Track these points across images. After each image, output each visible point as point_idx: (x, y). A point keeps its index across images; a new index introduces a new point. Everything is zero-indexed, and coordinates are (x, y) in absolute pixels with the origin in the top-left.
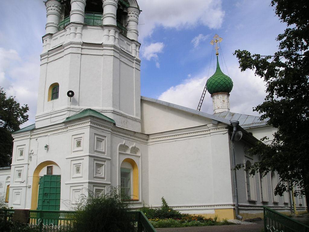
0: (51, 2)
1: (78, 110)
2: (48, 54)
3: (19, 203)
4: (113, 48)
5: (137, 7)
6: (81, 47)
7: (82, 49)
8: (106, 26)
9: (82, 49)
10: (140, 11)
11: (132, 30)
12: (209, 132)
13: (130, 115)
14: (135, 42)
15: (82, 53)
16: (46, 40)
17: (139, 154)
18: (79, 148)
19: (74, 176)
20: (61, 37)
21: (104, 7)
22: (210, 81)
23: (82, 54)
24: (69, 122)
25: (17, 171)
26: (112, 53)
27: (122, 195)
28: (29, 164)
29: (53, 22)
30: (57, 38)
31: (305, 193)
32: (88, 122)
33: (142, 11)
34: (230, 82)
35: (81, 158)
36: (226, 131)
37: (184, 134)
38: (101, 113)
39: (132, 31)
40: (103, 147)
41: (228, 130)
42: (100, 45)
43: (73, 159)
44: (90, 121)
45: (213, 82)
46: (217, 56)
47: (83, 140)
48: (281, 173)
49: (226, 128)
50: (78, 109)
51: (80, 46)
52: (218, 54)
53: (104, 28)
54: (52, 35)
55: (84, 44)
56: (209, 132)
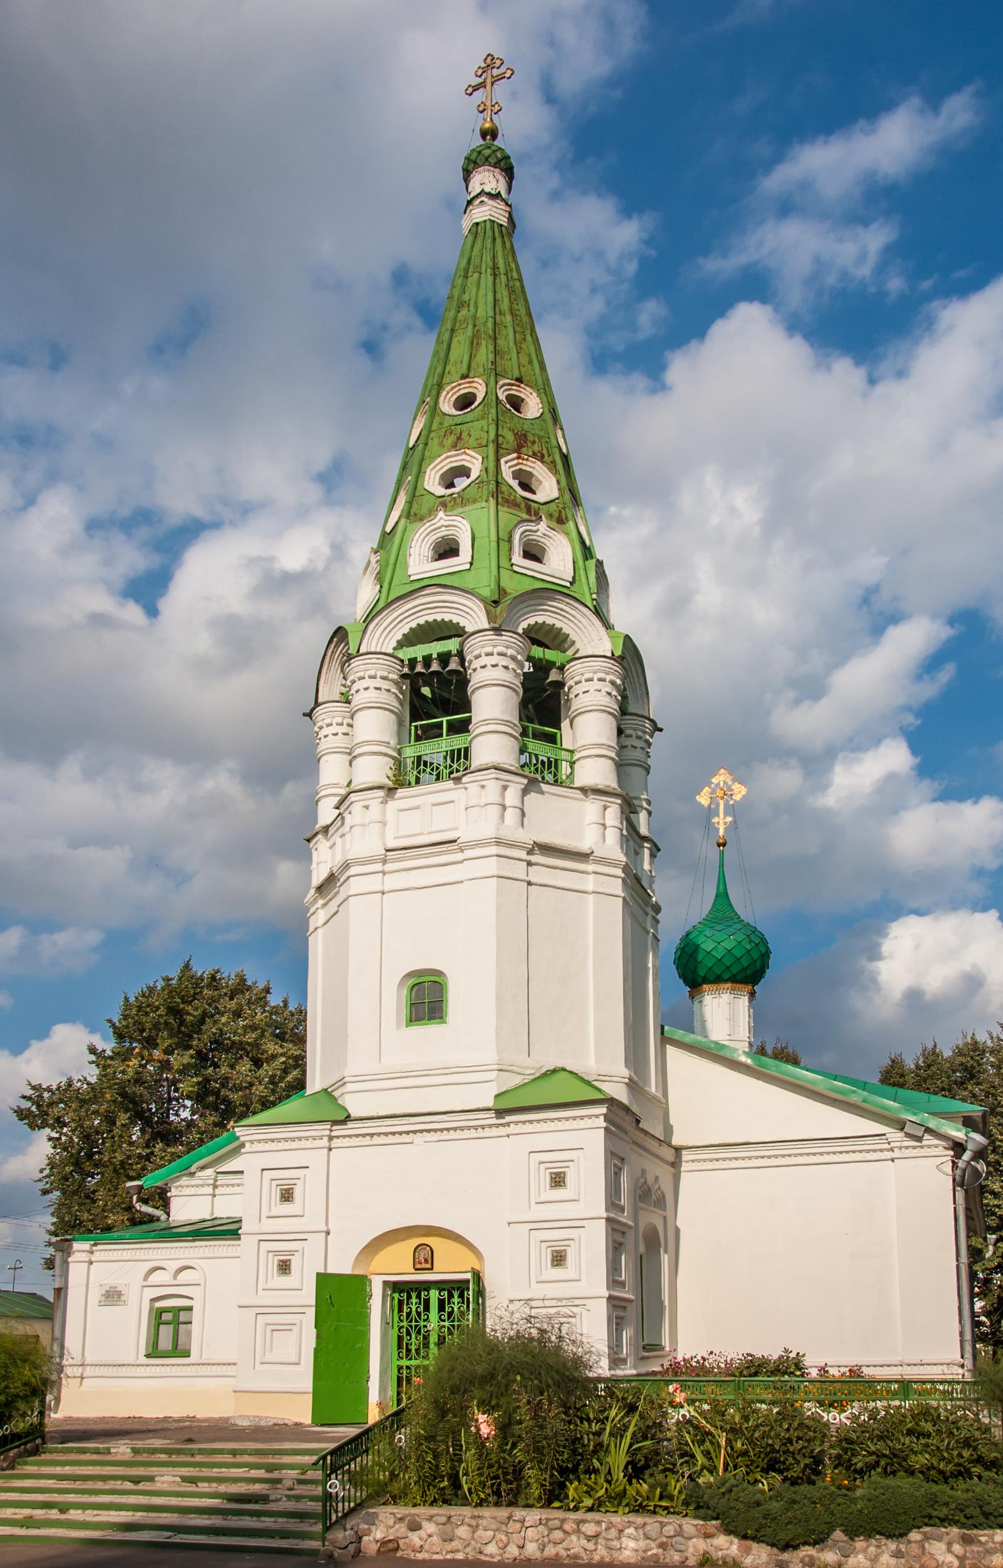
0: (374, 661)
1: (528, 1072)
2: (385, 862)
3: (294, 1359)
4: (494, 850)
7: (530, 864)
9: (530, 864)
12: (889, 1155)
15: (533, 880)
16: (483, 783)
19: (544, 1278)
21: (473, 692)
23: (529, 883)
24: (506, 1109)
25: (271, 1255)
26: (491, 866)
28: (328, 1233)
29: (387, 740)
32: (597, 1116)
35: (576, 1223)
37: (801, 1155)
43: (537, 1225)
44: (605, 1115)
48: (166, 1135)
50: (526, 1068)
51: (523, 854)
56: (889, 1155)
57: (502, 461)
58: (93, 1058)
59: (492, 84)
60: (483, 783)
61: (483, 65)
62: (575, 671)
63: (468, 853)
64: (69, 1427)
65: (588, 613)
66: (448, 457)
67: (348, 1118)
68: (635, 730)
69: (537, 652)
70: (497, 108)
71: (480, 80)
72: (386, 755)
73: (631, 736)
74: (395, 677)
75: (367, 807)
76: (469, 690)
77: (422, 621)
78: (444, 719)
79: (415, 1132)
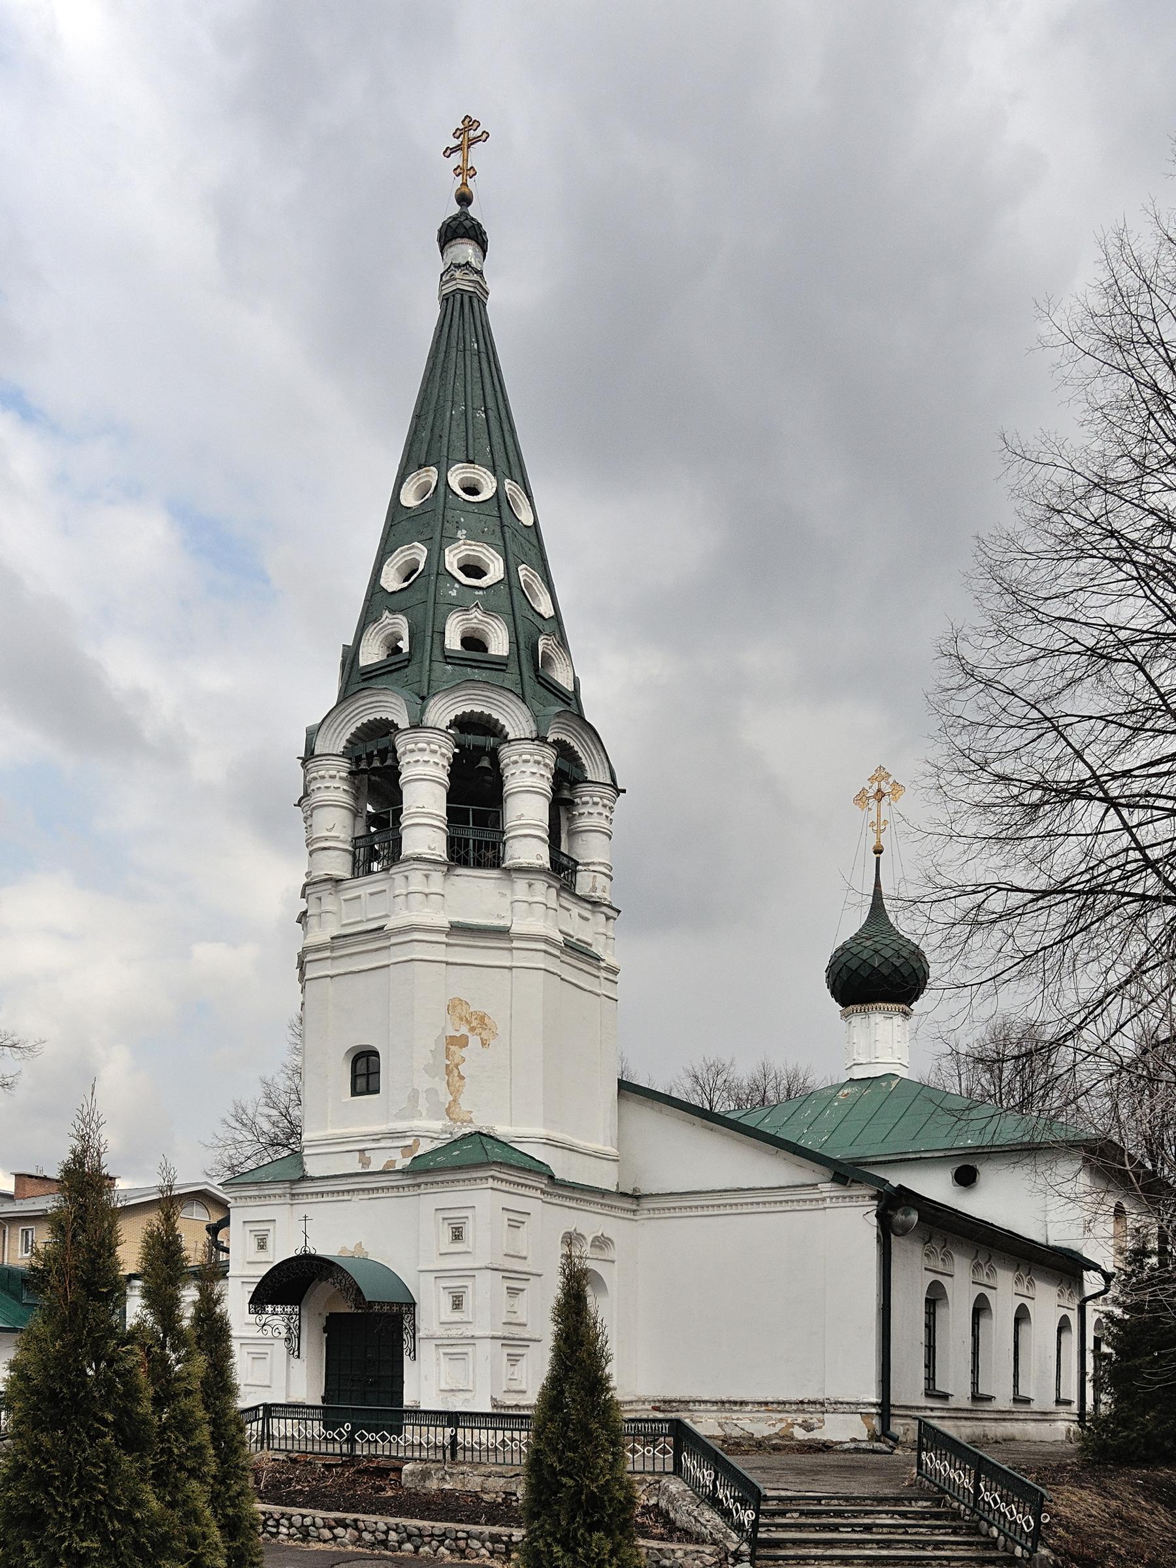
3: (267, 1383)
4: (543, 946)
5: (609, 782)
6: (445, 940)
8: (520, 870)
10: (619, 791)
11: (593, 863)
13: (587, 1144)
14: (604, 909)
16: (319, 895)
17: (610, 1254)
18: (458, 1247)
20: (371, 894)
22: (843, 959)
27: (216, 1341)
30: (359, 897)
31: (110, 1418)
33: (624, 791)
34: (916, 965)
36: (872, 1207)
38: (512, 1145)
39: (591, 868)
40: (523, 1241)
41: (876, 1202)
42: (502, 933)
45: (854, 964)
46: (878, 859)
47: (474, 1221)
49: (873, 1198)
52: (880, 852)
53: (514, 875)
54: (339, 881)
55: (458, 929)
57: (447, 551)
58: (282, 1083)
59: (469, 147)
60: (319, 895)
61: (461, 127)
62: (507, 754)
63: (394, 940)
64: (890, 1006)
65: (514, 698)
66: (402, 552)
67: (304, 1178)
68: (591, 797)
69: (472, 739)
70: (472, 172)
71: (458, 142)
72: (439, 828)
73: (587, 803)
74: (345, 775)
75: (320, 899)
76: (402, 780)
77: (365, 721)
78: (390, 809)
79: (353, 1191)
